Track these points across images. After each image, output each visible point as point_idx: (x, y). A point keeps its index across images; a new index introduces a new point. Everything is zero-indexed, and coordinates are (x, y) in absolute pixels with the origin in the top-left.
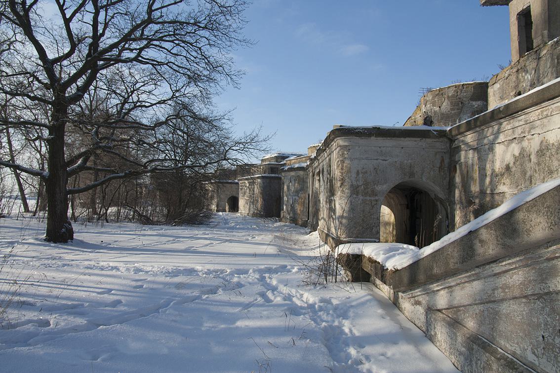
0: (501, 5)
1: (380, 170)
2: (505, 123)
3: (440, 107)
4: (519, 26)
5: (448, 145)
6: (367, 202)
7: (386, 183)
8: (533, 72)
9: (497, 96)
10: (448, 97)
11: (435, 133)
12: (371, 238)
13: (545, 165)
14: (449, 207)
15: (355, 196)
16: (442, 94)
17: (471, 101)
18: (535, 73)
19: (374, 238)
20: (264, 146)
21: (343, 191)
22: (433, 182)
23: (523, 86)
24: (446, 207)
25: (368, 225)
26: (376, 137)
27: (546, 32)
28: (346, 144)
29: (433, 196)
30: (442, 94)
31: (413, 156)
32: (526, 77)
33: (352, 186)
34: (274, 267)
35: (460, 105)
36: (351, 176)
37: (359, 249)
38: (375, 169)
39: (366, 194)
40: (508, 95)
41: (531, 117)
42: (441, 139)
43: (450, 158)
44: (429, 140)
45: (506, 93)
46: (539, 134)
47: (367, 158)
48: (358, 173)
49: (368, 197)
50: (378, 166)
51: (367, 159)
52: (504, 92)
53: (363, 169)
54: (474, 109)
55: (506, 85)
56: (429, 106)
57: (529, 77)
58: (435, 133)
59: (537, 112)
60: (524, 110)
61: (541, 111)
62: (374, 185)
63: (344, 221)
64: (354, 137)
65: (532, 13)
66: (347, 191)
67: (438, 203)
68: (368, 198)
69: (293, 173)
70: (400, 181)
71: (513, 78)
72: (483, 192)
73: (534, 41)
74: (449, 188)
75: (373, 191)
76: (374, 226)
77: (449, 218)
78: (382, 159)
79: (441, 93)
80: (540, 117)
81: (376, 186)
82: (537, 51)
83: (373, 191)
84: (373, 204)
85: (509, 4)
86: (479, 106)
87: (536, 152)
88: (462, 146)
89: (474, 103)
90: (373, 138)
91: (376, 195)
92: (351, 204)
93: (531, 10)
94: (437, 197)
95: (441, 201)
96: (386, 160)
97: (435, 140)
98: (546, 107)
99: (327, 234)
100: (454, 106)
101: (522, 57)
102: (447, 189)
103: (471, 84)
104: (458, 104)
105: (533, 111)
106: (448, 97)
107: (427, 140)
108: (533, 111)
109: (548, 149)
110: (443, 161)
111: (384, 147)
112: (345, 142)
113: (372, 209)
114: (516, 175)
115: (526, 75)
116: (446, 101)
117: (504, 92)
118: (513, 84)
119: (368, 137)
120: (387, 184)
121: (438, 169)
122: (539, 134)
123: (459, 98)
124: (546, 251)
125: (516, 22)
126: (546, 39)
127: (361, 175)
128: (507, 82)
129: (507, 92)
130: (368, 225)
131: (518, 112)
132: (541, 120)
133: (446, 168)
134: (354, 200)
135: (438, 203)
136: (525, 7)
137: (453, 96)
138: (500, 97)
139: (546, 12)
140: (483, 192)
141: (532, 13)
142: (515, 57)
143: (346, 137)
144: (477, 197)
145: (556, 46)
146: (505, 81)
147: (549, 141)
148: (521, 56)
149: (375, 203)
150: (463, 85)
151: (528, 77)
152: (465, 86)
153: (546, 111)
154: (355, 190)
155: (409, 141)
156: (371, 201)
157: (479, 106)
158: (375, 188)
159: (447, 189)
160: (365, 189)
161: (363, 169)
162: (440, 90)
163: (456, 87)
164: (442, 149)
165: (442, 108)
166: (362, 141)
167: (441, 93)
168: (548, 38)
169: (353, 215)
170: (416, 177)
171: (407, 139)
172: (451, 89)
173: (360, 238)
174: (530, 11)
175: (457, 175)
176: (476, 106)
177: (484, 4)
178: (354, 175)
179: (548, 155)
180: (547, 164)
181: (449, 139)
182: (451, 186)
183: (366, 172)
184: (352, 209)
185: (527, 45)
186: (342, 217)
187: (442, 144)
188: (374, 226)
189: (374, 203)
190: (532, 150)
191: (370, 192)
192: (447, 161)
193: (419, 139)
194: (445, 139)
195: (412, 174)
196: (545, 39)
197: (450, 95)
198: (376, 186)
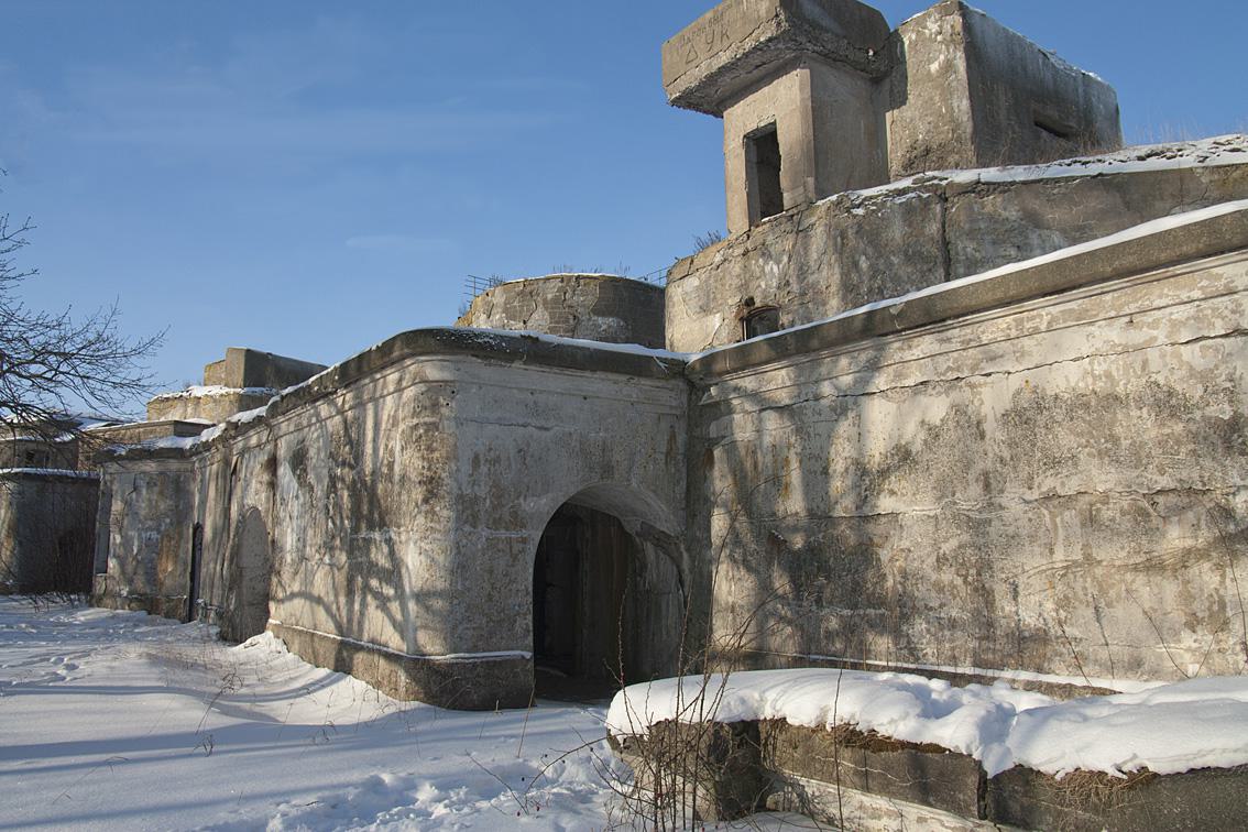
0: (705, 112)
1: (532, 456)
2: (896, 345)
3: (525, 322)
4: (748, 161)
5: (684, 399)
6: (500, 546)
7: (548, 492)
8: (785, 259)
9: (693, 303)
10: (545, 302)
11: (661, 364)
12: (512, 649)
13: (1034, 445)
14: (685, 555)
15: (467, 528)
16: (531, 293)
17: (594, 314)
18: (789, 261)
19: (517, 649)
20: (130, 372)
21: (434, 513)
22: (654, 492)
23: (760, 286)
24: (675, 554)
25: (503, 611)
26: (525, 363)
27: (811, 180)
28: (446, 375)
29: (632, 526)
30: (531, 293)
31: (610, 420)
32: (767, 269)
33: (460, 498)
34: (351, 794)
35: (571, 321)
36: (458, 470)
37: (743, 701)
38: (520, 451)
39: (496, 523)
40: (721, 304)
41: (983, 333)
42: (673, 382)
43: (689, 430)
44: (646, 383)
45: (715, 298)
46: (1009, 373)
47: (500, 418)
48: (476, 461)
49: (503, 531)
50: (528, 445)
51: (499, 422)
52: (712, 296)
53: (491, 449)
54: (599, 333)
55: (716, 281)
56: (498, 317)
57: (775, 268)
58: (661, 364)
59: (1003, 324)
60: (967, 314)
61: (1014, 320)
62: (518, 498)
63: (438, 604)
64: (470, 357)
65: (781, 138)
66: (445, 513)
67: (649, 548)
68: (503, 534)
69: (151, 467)
70: (580, 488)
71: (736, 268)
72: (820, 516)
73: (785, 195)
74: (687, 506)
75: (516, 512)
76: (518, 614)
77: (687, 583)
78: (538, 425)
79: (528, 291)
80: (1013, 333)
81: (521, 500)
82: (792, 216)
83: (515, 514)
84: (515, 551)
85: (725, 114)
86: (609, 327)
87: (999, 416)
88: (735, 402)
89: (600, 320)
90: (517, 364)
91: (523, 526)
92: (459, 553)
93: (778, 132)
94: (649, 532)
95: (662, 541)
96: (547, 429)
97: (660, 384)
98: (1033, 310)
99: (342, 642)
100: (557, 322)
101: (757, 226)
102: (683, 509)
103: (595, 278)
104: (567, 321)
105: (988, 320)
106: (545, 302)
107: (643, 381)
108: (988, 320)
109: (1040, 409)
110: (673, 437)
111: (541, 392)
112: (442, 369)
113: (513, 566)
114: (934, 472)
115: (766, 263)
116: (540, 309)
117: (712, 296)
118: (736, 282)
119: (507, 361)
120: (550, 495)
121: (663, 457)
122: (1009, 373)
123: (570, 307)
124: (63, 618)
125: (742, 152)
126: (811, 195)
127: (484, 469)
128: (715, 276)
129: (719, 296)
130: (503, 611)
131: (944, 320)
132: (1016, 341)
133: (679, 457)
134: (465, 541)
135: (649, 548)
136: (762, 124)
137: (556, 300)
138: (701, 307)
139: (810, 142)
140: (820, 516)
141: (779, 138)
142: (738, 219)
143: (447, 357)
144: (795, 529)
145: (837, 212)
146: (714, 272)
147: (1044, 389)
148: (753, 222)
149: (521, 546)
150: (578, 278)
151: (772, 269)
152: (582, 282)
153: (1030, 319)
154: (468, 511)
155: (603, 380)
156: (509, 541)
157: (609, 327)
158: (520, 505)
159: (683, 509)
160: (494, 508)
161: (491, 449)
162: (526, 283)
163: (562, 281)
164: (671, 407)
165: (529, 324)
166: (487, 372)
167: (529, 289)
168: (816, 193)
169: (463, 584)
170: (616, 476)
171: (599, 374)
172: (551, 284)
173: (484, 651)
174: (775, 131)
175: (716, 473)
176: (604, 327)
177: (675, 102)
178: (466, 468)
179: (1042, 423)
180: (1040, 444)
181: (691, 384)
182: (696, 505)
183: (497, 460)
184: (460, 567)
185: (765, 199)
186: (422, 597)
187: (673, 394)
188: (518, 614)
189: (517, 547)
190: (985, 410)
191: (507, 517)
192: (681, 438)
193: (624, 378)
194: (681, 384)
195: (608, 470)
196: (810, 195)
197: (550, 296)
198: (521, 500)
